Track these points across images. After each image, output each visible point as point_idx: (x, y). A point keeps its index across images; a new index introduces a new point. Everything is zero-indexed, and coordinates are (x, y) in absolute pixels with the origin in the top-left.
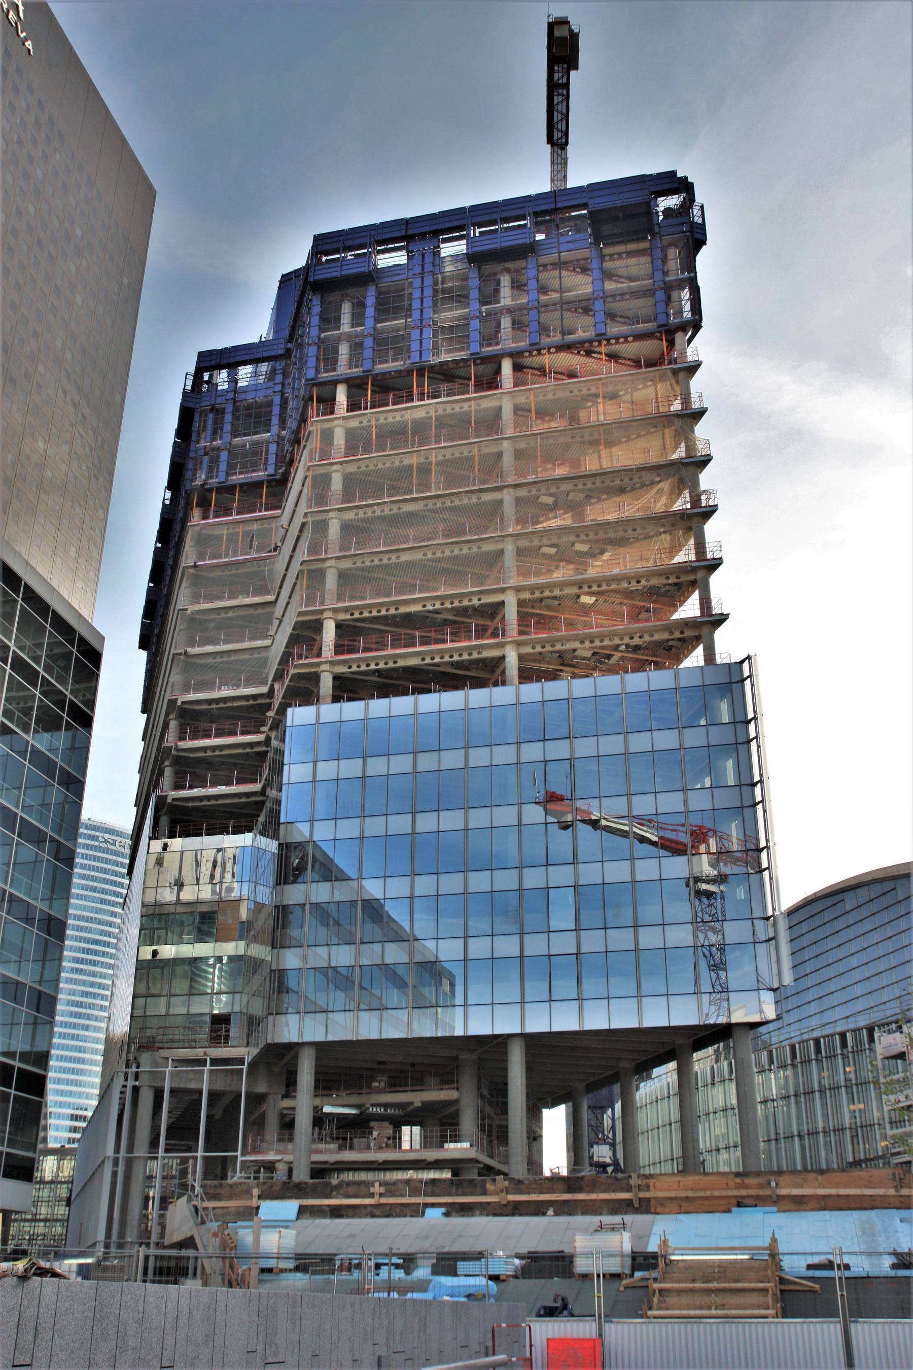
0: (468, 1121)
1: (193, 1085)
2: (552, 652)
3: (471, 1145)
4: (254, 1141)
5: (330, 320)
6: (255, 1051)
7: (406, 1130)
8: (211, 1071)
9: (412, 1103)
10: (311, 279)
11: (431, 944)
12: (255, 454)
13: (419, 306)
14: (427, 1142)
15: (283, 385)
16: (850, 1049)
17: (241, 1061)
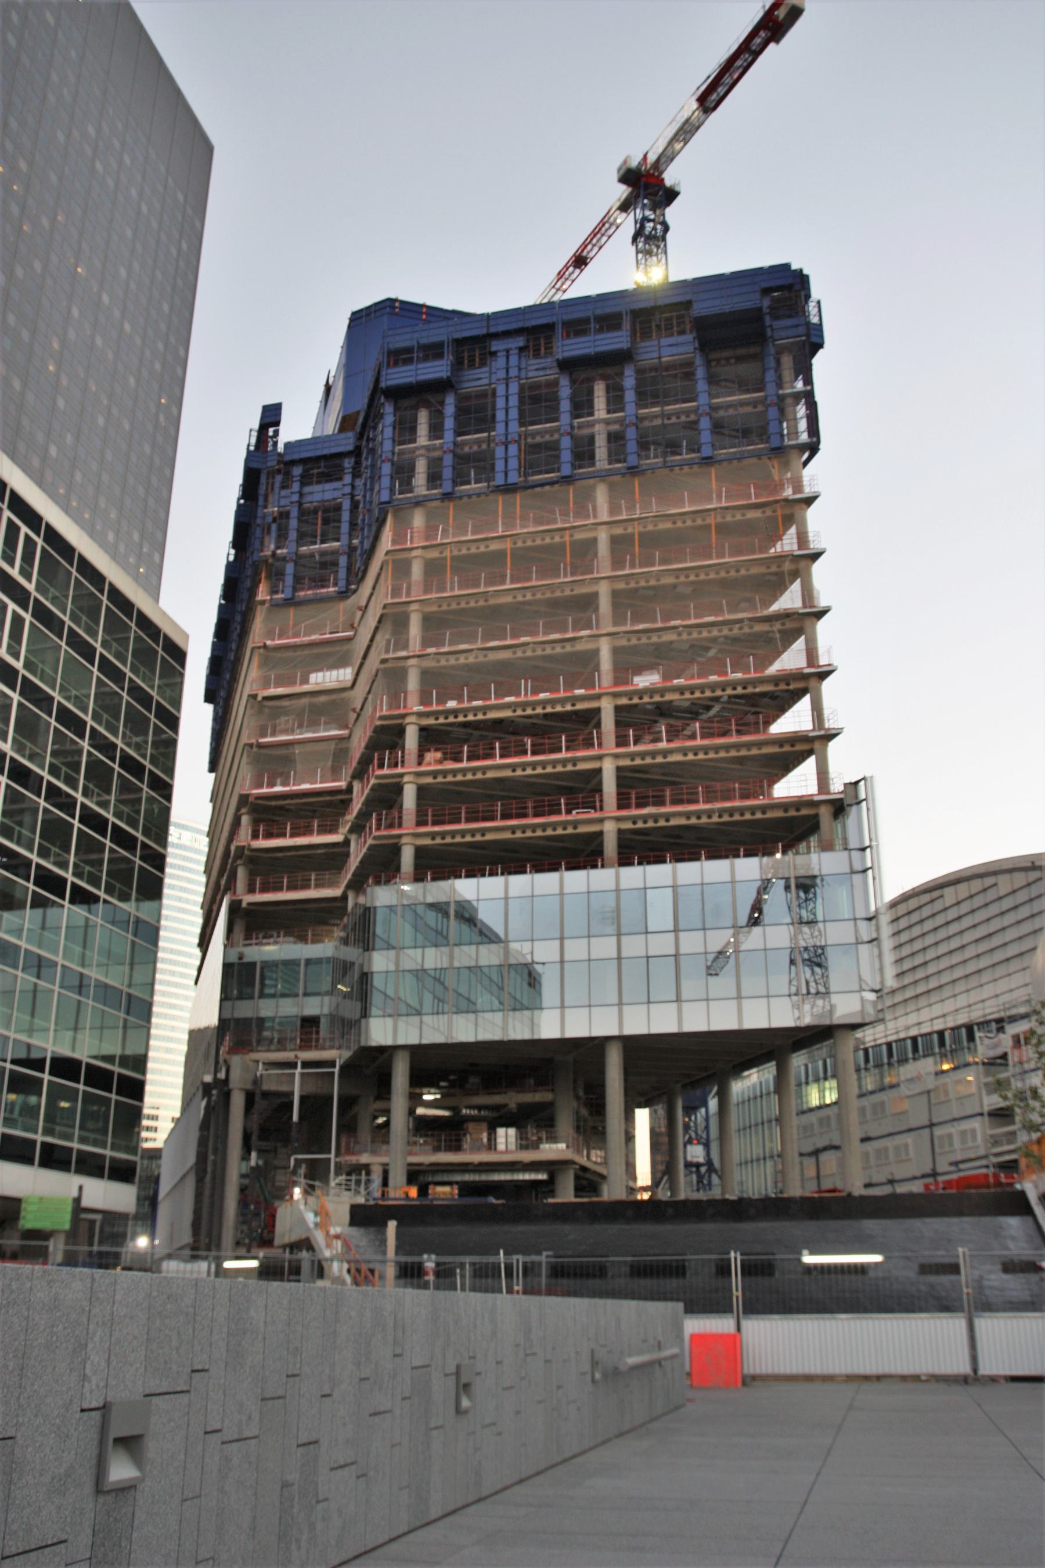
0: (565, 1123)
1: (284, 1088)
2: (648, 645)
3: (568, 1147)
4: (348, 1144)
5: (406, 430)
6: (347, 1054)
7: (501, 1131)
8: (302, 1075)
9: (505, 1106)
10: (383, 385)
11: (526, 947)
12: (323, 565)
13: (503, 455)
14: (525, 1144)
15: (353, 487)
16: (948, 1048)
17: (332, 1064)
